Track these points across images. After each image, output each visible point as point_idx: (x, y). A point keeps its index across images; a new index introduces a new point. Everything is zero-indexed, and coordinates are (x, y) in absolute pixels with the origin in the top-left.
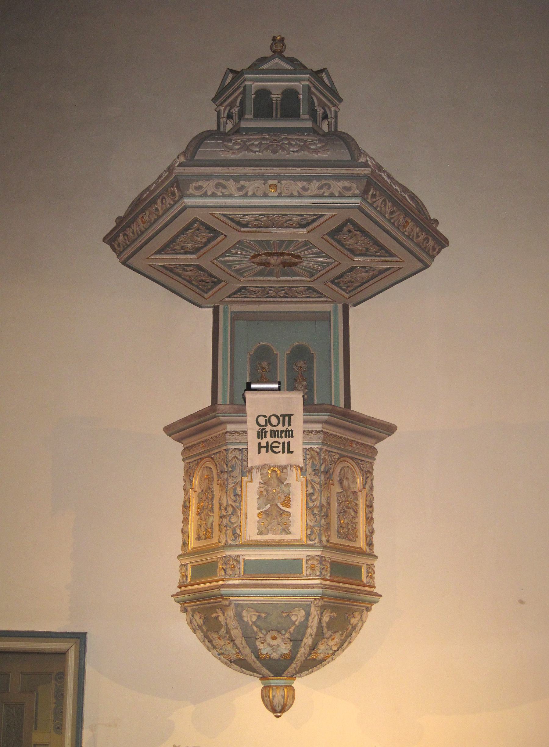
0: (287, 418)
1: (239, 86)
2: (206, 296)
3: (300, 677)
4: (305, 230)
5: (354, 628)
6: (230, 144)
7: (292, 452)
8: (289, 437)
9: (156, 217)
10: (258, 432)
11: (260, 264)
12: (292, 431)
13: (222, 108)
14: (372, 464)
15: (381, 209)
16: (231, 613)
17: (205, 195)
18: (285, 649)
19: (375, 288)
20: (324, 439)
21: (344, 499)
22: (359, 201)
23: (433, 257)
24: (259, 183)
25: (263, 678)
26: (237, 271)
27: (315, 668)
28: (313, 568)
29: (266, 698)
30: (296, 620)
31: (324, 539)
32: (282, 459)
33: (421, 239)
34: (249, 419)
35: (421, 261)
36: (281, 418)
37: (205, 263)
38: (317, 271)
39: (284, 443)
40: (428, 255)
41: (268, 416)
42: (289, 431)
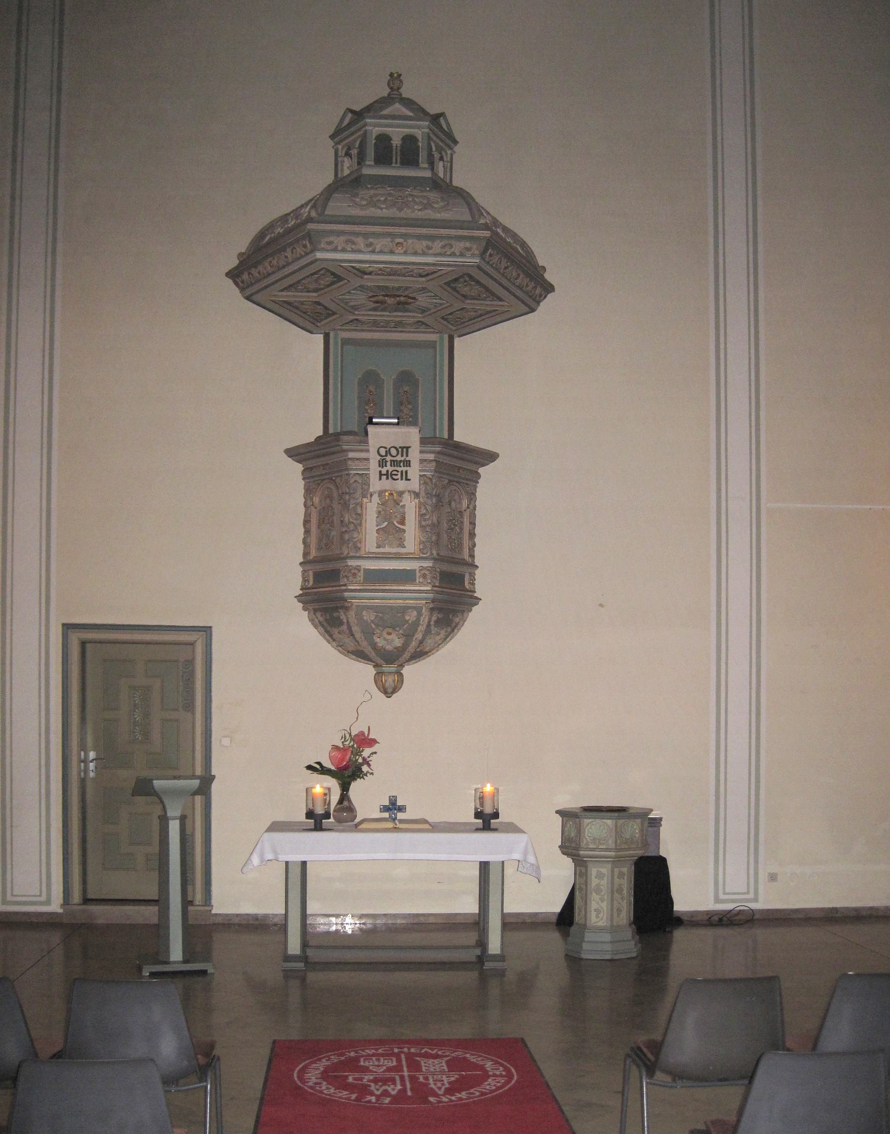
0: (405, 450)
1: (359, 130)
2: (319, 324)
3: (409, 665)
4: (424, 279)
5: (457, 624)
6: (358, 200)
7: (409, 480)
8: (407, 466)
9: (285, 264)
10: (379, 461)
11: (377, 302)
12: (410, 461)
13: (340, 147)
14: (475, 487)
15: (496, 265)
16: (352, 614)
17: (335, 250)
18: (398, 642)
19: (484, 324)
20: (436, 467)
21: (451, 518)
22: (478, 261)
23: (538, 303)
24: (386, 241)
25: (376, 666)
26: (352, 307)
27: (421, 658)
28: (424, 576)
29: (379, 683)
30: (409, 619)
31: (434, 552)
32: (401, 485)
33: (529, 288)
34: (371, 449)
35: (526, 305)
36: (400, 450)
37: (325, 300)
38: (430, 310)
39: (402, 472)
40: (534, 300)
41: (389, 447)
42: (407, 461)
